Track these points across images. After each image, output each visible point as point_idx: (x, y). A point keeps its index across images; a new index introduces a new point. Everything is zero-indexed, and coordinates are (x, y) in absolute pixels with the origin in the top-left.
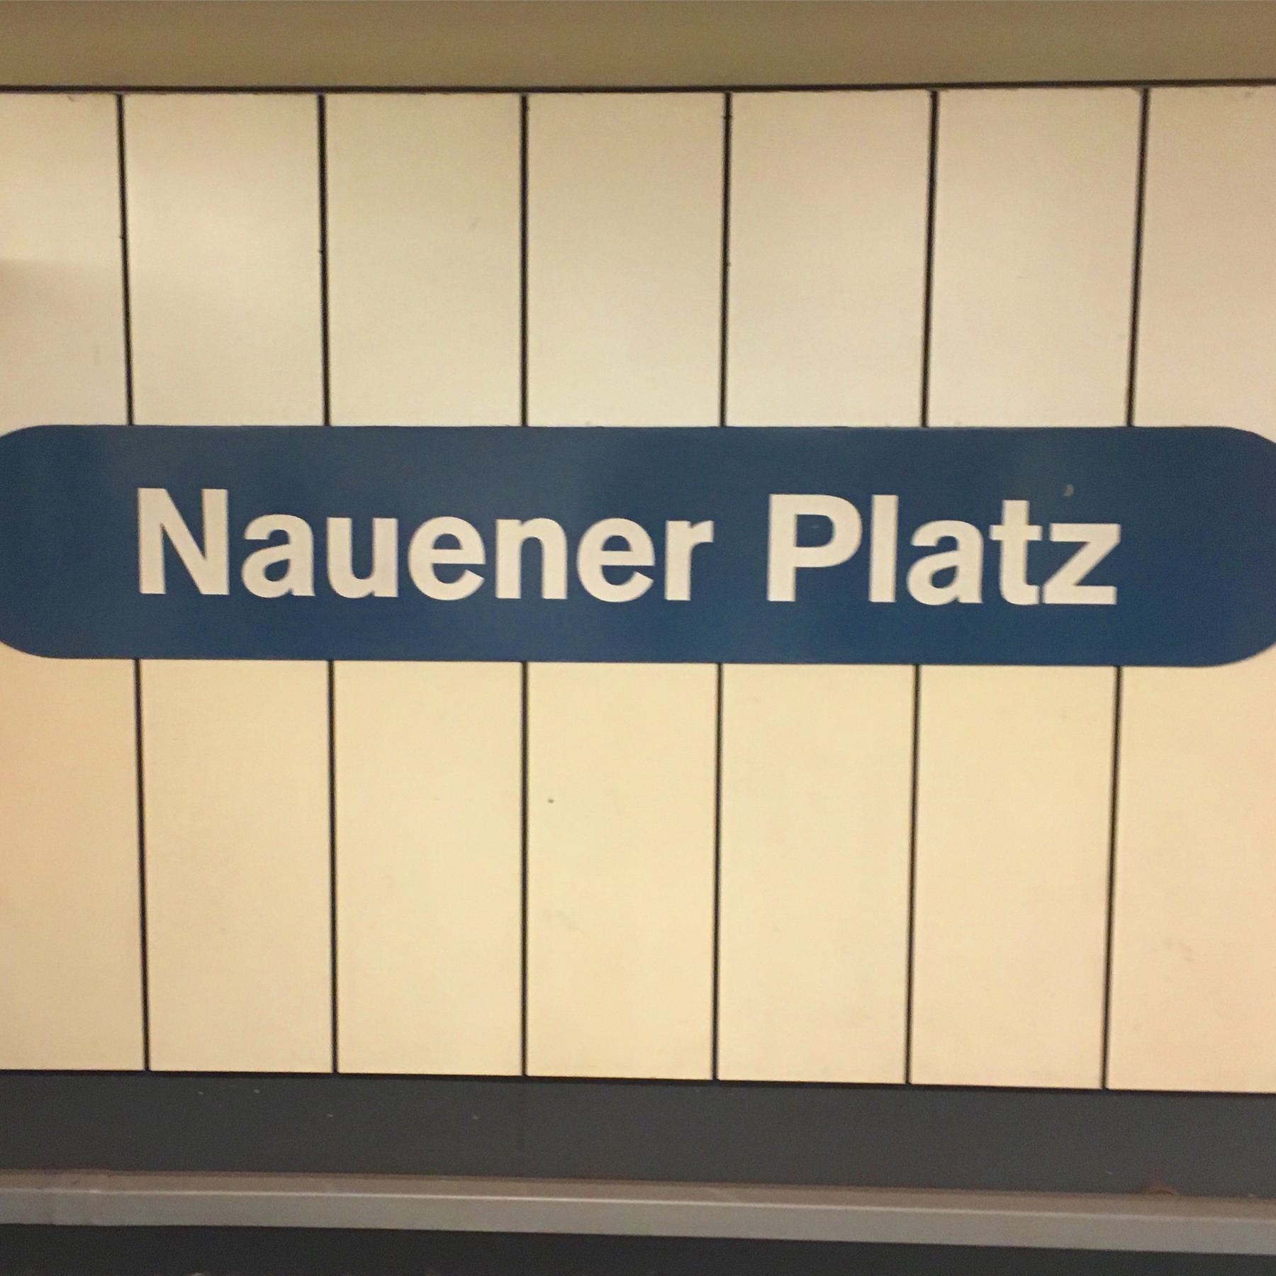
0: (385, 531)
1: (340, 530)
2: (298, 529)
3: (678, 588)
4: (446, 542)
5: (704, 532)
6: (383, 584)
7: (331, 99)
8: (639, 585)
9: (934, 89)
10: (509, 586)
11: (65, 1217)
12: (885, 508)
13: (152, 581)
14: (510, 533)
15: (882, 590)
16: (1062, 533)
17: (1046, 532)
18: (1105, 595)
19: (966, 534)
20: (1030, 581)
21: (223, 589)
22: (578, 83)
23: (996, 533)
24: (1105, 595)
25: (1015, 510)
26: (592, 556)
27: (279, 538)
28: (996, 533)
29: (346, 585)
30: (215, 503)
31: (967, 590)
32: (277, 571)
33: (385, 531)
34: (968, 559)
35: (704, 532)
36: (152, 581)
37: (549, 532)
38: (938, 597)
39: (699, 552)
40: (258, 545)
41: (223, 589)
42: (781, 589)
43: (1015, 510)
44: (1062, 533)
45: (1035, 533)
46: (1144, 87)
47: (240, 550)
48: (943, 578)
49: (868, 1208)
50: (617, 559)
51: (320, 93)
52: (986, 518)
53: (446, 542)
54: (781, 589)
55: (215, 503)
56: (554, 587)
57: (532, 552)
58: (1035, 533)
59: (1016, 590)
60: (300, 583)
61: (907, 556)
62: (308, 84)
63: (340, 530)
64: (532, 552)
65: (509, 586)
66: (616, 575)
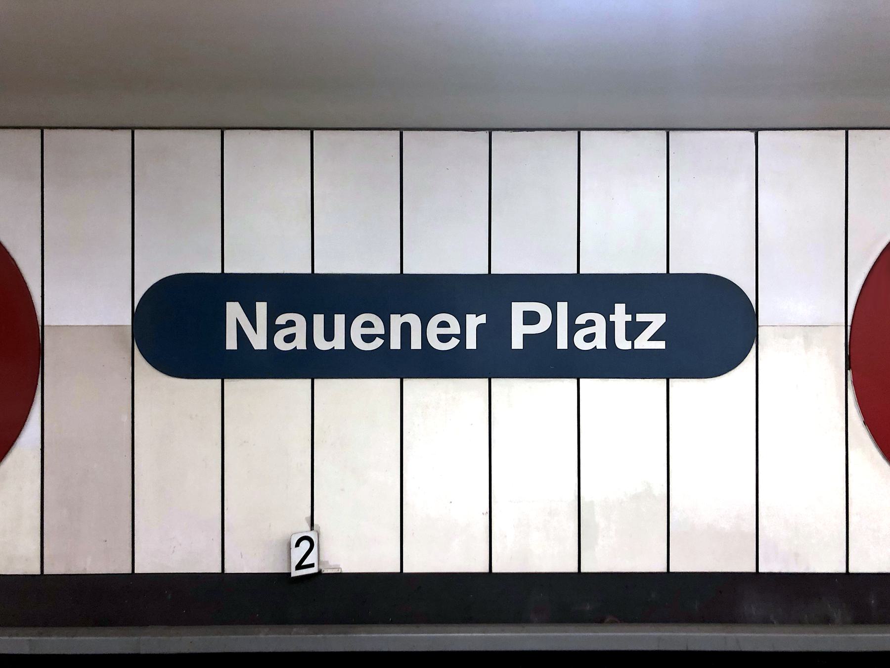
0: (340, 320)
1: (319, 320)
2: (300, 320)
3: (471, 343)
4: (444, 324)
5: (482, 319)
6: (339, 343)
7: (406, 134)
8: (454, 343)
9: (847, 130)
10: (395, 343)
11: (144, 650)
12: (562, 308)
13: (231, 344)
14: (396, 321)
15: (562, 343)
16: (641, 317)
17: (634, 318)
18: (661, 345)
19: (599, 318)
20: (627, 339)
21: (264, 346)
22: (776, 127)
23: (612, 318)
24: (661, 345)
25: (620, 308)
26: (433, 331)
27: (591, 323)
28: (612, 318)
29: (321, 344)
30: (261, 308)
31: (600, 343)
32: (589, 338)
33: (340, 320)
34: (600, 329)
35: (482, 319)
36: (231, 344)
37: (413, 320)
38: (288, 347)
39: (480, 327)
40: (582, 326)
41: (264, 346)
42: (517, 343)
43: (620, 308)
44: (641, 317)
45: (629, 318)
46: (668, 131)
47: (272, 329)
48: (289, 339)
49: (555, 634)
50: (368, 331)
51: (847, 130)
52: (607, 312)
53: (444, 324)
54: (517, 343)
55: (261, 308)
56: (416, 344)
57: (406, 329)
58: (629, 318)
59: (622, 344)
60: (300, 343)
61: (573, 329)
62: (842, 126)
63: (319, 320)
64: (406, 329)
65: (395, 343)
66: (368, 338)
